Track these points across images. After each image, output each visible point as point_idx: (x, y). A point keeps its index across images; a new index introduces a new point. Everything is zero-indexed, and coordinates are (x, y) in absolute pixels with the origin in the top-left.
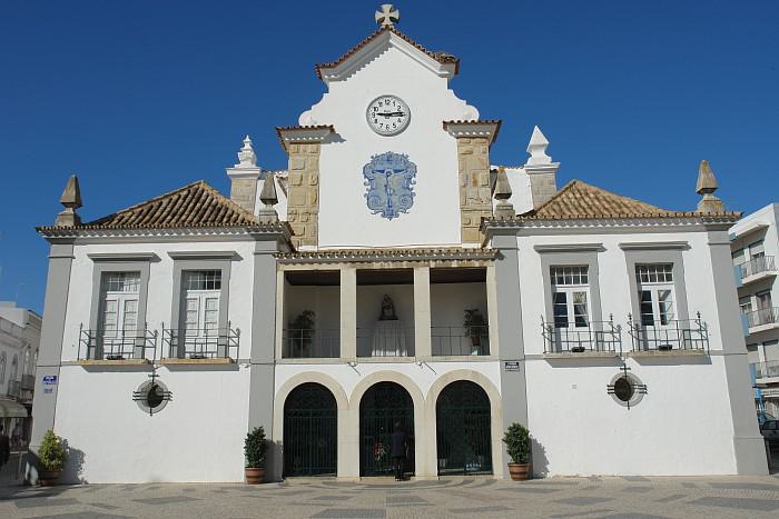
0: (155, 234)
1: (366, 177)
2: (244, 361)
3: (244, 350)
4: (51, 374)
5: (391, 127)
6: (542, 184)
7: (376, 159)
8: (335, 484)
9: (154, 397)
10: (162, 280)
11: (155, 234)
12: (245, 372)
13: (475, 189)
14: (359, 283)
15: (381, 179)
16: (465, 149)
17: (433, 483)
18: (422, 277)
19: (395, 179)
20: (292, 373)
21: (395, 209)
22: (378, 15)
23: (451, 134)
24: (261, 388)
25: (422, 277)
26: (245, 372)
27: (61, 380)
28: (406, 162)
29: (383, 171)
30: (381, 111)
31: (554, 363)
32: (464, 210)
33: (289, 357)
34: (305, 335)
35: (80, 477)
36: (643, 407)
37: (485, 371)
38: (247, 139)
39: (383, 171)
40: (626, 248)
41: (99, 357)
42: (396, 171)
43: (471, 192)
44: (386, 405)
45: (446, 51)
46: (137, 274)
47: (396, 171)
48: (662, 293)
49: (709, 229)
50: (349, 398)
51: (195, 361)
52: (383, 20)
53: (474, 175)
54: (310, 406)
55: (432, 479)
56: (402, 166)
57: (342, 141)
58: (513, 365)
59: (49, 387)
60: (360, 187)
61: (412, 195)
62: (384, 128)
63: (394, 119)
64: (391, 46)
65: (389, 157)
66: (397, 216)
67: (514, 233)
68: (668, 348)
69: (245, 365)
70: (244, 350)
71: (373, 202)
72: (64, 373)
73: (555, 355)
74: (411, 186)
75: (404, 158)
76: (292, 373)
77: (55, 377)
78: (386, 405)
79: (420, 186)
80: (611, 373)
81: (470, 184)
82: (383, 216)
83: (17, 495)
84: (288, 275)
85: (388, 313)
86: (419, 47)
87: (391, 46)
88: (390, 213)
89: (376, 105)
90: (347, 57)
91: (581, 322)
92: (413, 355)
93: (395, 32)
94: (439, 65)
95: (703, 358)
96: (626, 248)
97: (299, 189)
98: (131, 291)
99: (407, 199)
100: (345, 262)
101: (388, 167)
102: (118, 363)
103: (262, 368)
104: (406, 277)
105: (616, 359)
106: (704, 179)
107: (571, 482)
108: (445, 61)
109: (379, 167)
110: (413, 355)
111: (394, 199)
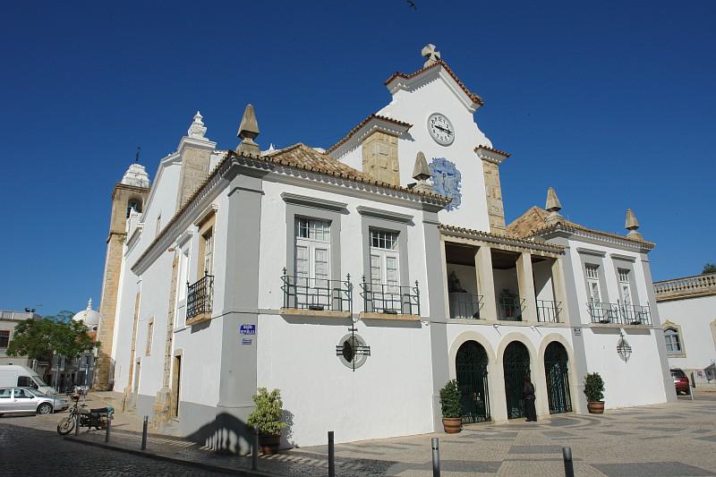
0: (354, 187)
2: (425, 319)
4: (248, 322)
9: (349, 351)
10: (352, 229)
11: (334, 183)
12: (426, 329)
14: (533, 262)
16: (487, 169)
19: (449, 180)
20: (459, 332)
22: (425, 51)
23: (479, 156)
24: (438, 342)
26: (426, 329)
27: (259, 330)
28: (454, 169)
29: (440, 172)
30: (437, 124)
31: (291, 319)
34: (461, 296)
35: (290, 441)
37: (566, 337)
38: (198, 114)
39: (440, 172)
41: (301, 312)
43: (493, 202)
44: (516, 355)
45: (479, 95)
46: (329, 223)
47: (449, 174)
51: (387, 316)
52: (429, 55)
53: (493, 189)
54: (471, 355)
57: (413, 140)
58: (577, 331)
59: (248, 337)
63: (444, 134)
64: (439, 76)
67: (566, 236)
69: (426, 323)
72: (262, 322)
76: (459, 332)
77: (254, 326)
78: (516, 355)
80: (340, 333)
86: (460, 85)
87: (439, 76)
90: (451, 75)
93: (446, 68)
94: (471, 103)
95: (417, 324)
97: (384, 172)
98: (318, 239)
100: (483, 241)
102: (315, 315)
105: (349, 321)
106: (631, 221)
107: (622, 413)
108: (477, 101)
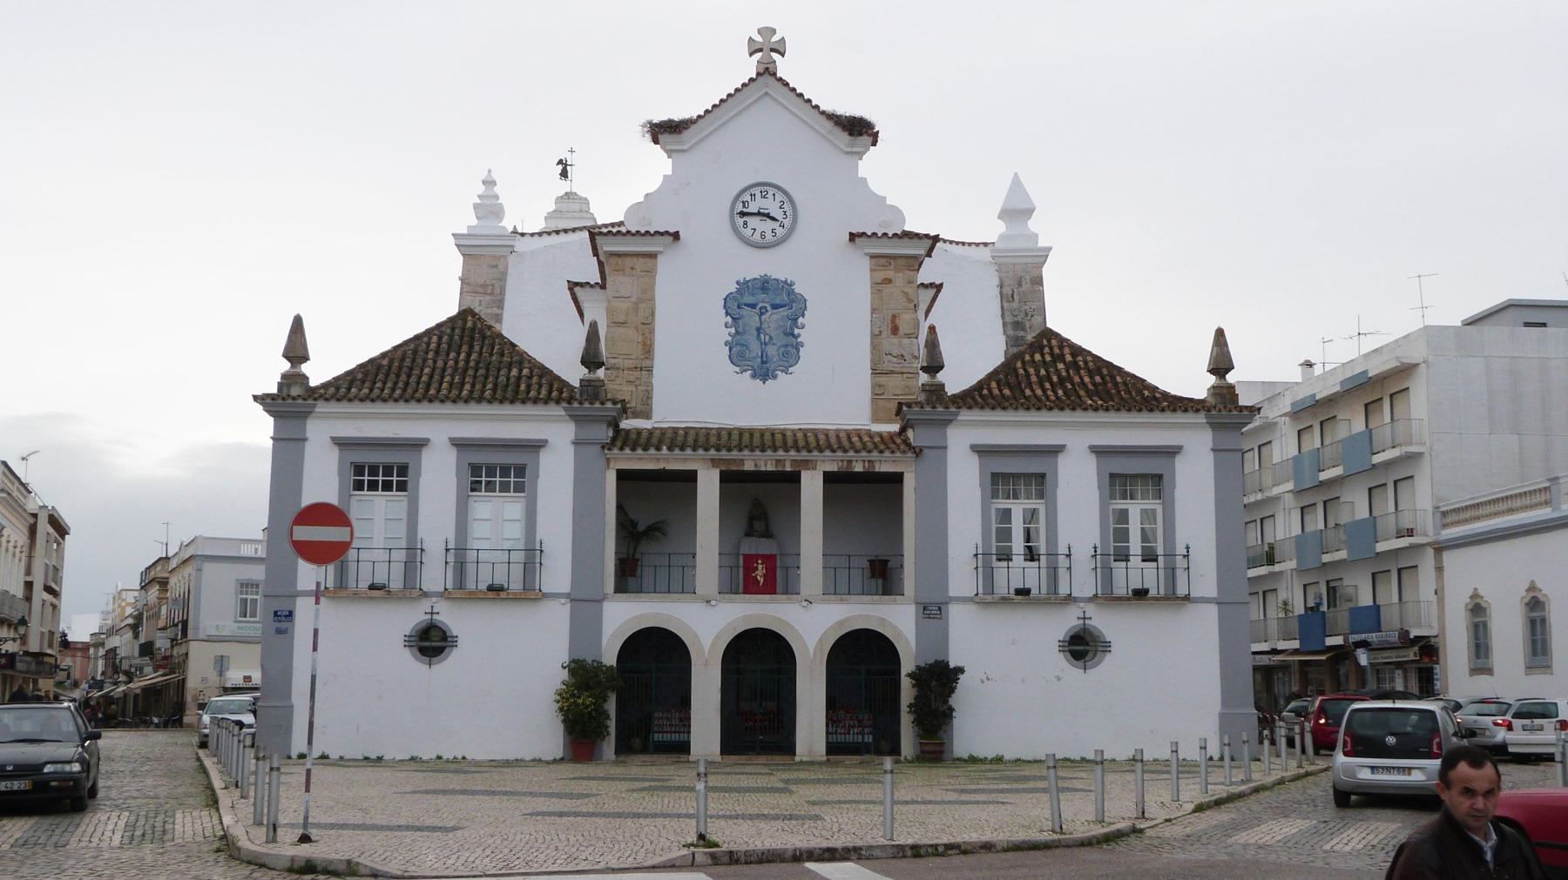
1: (727, 314)
3: (557, 574)
5: (769, 235)
6: (1020, 285)
7: (744, 286)
13: (895, 340)
15: (752, 319)
17: (820, 763)
18: (812, 487)
19: (773, 319)
25: (812, 487)
28: (791, 293)
29: (753, 306)
32: (875, 372)
36: (1107, 667)
39: (753, 306)
40: (1100, 452)
42: (775, 307)
48: (201, 771)
49: (304, 823)
55: (819, 759)
58: (932, 611)
59: (283, 625)
60: (718, 330)
61: (798, 346)
62: (757, 236)
65: (765, 284)
66: (775, 377)
68: (1023, 592)
70: (557, 574)
71: (737, 354)
73: (989, 598)
74: (796, 331)
75: (787, 286)
79: (811, 331)
81: (886, 332)
82: (754, 376)
84: (623, 476)
85: (758, 526)
88: (764, 373)
89: (747, 197)
91: (1031, 555)
92: (50, 515)
96: (1100, 452)
99: (791, 352)
101: (762, 299)
103: (584, 604)
109: (749, 299)
110: (50, 515)
111: (771, 350)
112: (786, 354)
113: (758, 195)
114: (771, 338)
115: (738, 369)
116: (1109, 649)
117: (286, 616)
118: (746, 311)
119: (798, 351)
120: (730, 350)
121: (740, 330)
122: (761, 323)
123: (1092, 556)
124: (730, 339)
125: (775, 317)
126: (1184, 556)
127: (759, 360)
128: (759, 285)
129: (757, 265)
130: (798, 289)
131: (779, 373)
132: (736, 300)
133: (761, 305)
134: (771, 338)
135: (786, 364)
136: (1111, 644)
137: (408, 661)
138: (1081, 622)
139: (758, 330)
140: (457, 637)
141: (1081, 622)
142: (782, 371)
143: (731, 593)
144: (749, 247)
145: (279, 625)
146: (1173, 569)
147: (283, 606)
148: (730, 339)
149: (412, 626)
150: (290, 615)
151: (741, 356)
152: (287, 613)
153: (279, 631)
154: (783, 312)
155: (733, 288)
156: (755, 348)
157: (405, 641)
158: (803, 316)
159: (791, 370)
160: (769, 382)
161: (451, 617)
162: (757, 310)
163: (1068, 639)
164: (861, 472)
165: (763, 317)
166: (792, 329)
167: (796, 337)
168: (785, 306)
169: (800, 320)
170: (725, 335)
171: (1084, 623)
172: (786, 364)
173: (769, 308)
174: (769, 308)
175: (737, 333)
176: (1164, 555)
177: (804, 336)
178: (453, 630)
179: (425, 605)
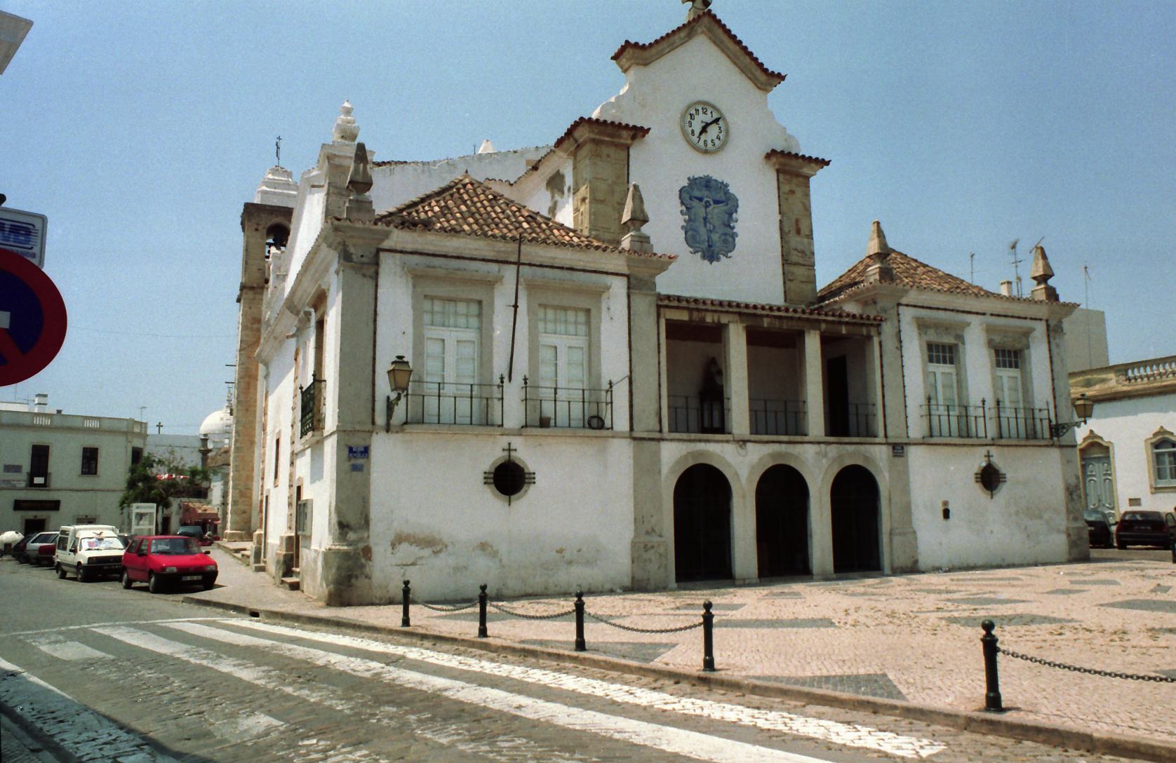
1: (682, 203)
7: (693, 182)
8: (893, 586)
13: (799, 239)
15: (699, 209)
19: (716, 211)
21: (716, 250)
24: (645, 469)
28: (727, 193)
29: (700, 199)
33: (334, 606)
39: (700, 199)
42: (717, 202)
50: (293, 370)
56: (721, 196)
59: (360, 461)
61: (734, 236)
65: (707, 183)
66: (718, 259)
75: (723, 187)
83: (268, 643)
104: (716, 334)
109: (697, 193)
111: (715, 237)
112: (725, 241)
113: (701, 111)
114: (714, 227)
115: (691, 250)
116: (486, 475)
117: (361, 452)
118: (695, 203)
119: (734, 240)
120: (686, 233)
121: (693, 217)
122: (707, 214)
123: (522, 388)
124: (684, 224)
125: (716, 211)
126: (499, 386)
127: (706, 244)
128: (704, 183)
129: (703, 167)
130: (732, 190)
131: (721, 256)
132: (688, 193)
133: (706, 199)
134: (714, 227)
135: (726, 249)
136: (535, 476)
137: (490, 499)
138: (506, 453)
139: (705, 219)
140: (534, 473)
141: (506, 453)
142: (724, 255)
143: (1108, 457)
144: (693, 150)
145: (354, 461)
146: (598, 403)
147: (357, 442)
148: (684, 224)
149: (490, 463)
150: (366, 451)
151: (694, 237)
152: (363, 450)
153: (356, 468)
154: (722, 207)
155: (686, 183)
156: (703, 231)
157: (534, 478)
158: (736, 211)
159: (729, 254)
160: (715, 263)
161: (527, 454)
162: (703, 203)
163: (493, 470)
164: (343, 296)
165: (708, 209)
166: (729, 221)
167: (733, 228)
168: (722, 202)
169: (734, 215)
170: (681, 220)
171: (510, 456)
172: (726, 249)
173: (712, 203)
174: (712, 203)
175: (690, 220)
176: (538, 387)
177: (739, 228)
178: (529, 466)
179: (504, 441)
